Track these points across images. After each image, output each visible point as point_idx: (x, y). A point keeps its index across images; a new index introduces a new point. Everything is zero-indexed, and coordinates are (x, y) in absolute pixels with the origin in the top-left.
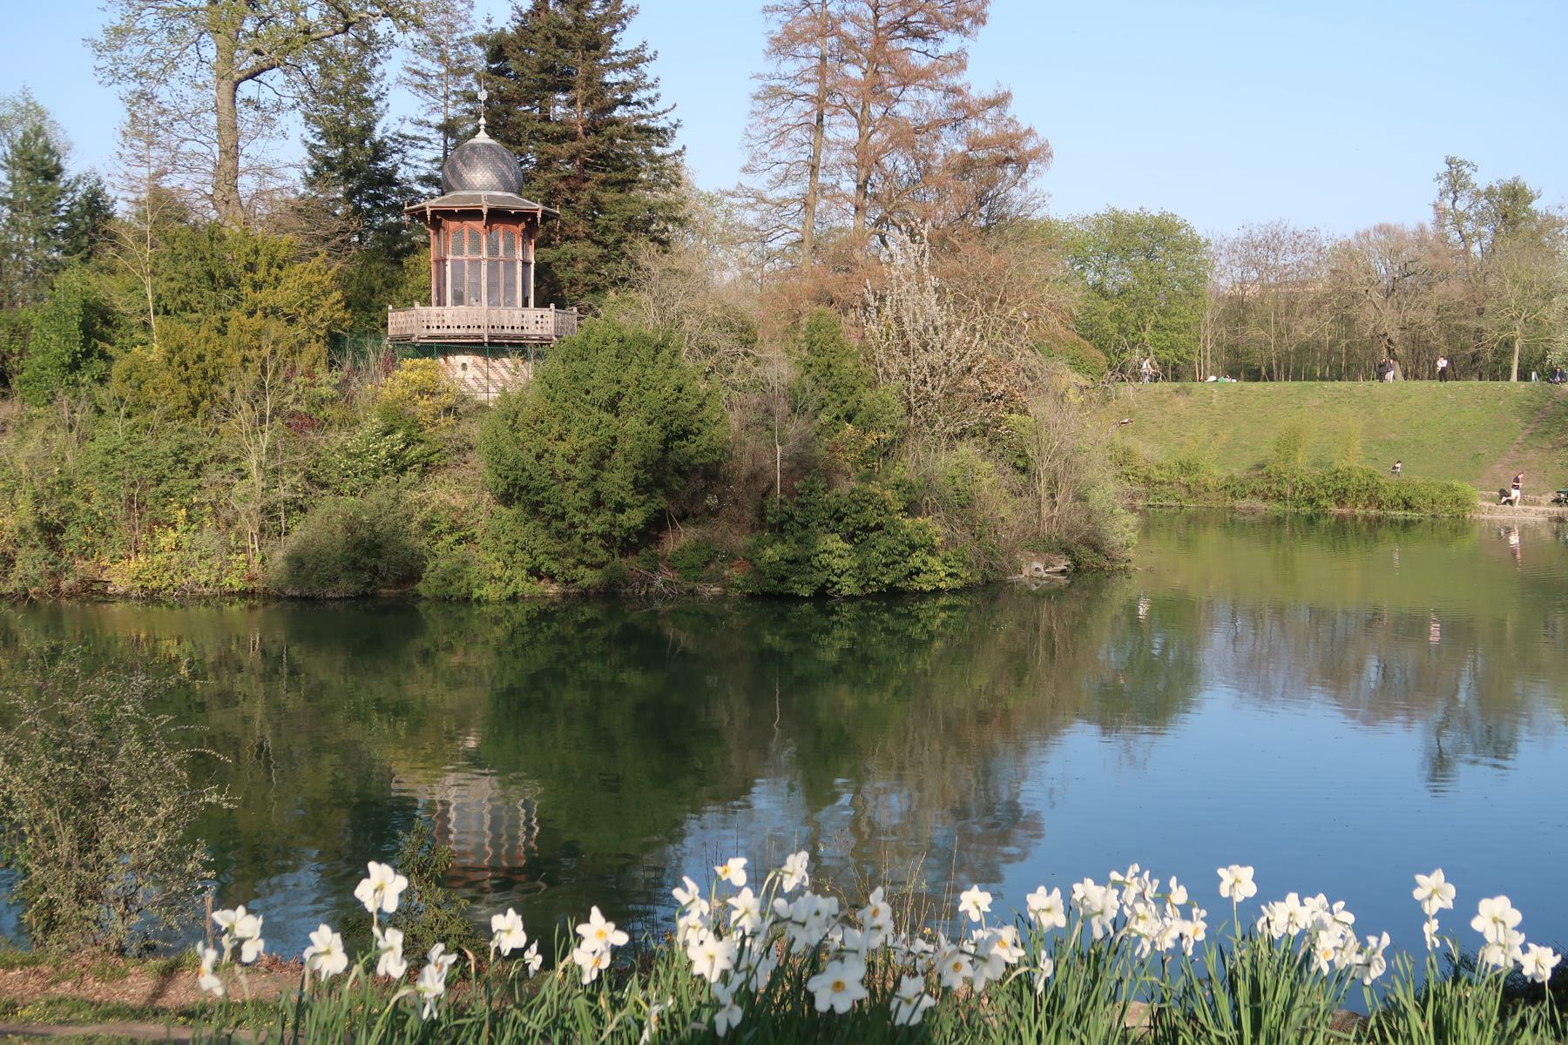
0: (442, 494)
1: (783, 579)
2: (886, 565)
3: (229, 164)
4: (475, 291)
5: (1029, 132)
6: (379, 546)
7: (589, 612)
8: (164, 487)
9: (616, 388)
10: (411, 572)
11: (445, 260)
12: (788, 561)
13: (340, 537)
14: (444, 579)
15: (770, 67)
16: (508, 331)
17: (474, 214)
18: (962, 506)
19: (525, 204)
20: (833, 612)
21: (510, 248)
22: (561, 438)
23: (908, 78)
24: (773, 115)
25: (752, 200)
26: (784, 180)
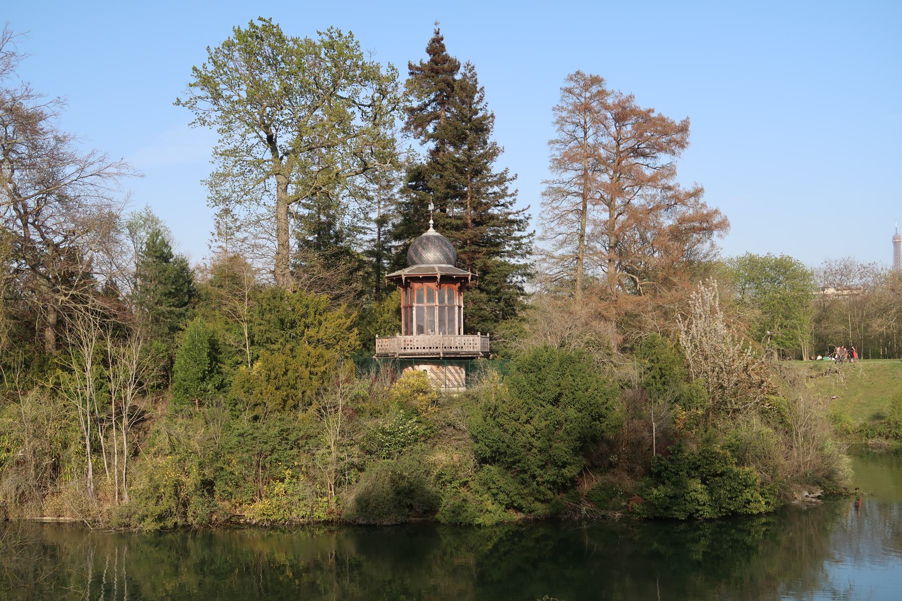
0: (442, 457)
1: (667, 509)
2: (730, 499)
3: (285, 252)
4: (432, 326)
5: (716, 212)
6: (412, 491)
7: (542, 531)
8: (275, 456)
9: (558, 390)
10: (431, 506)
11: (411, 307)
12: (670, 498)
13: (387, 486)
14: (453, 512)
15: (555, 176)
16: (453, 350)
17: (432, 279)
18: (763, 457)
19: (461, 272)
20: (698, 529)
21: (451, 298)
22: (527, 422)
23: (640, 181)
24: (555, 205)
25: (544, 257)
26: (562, 244)
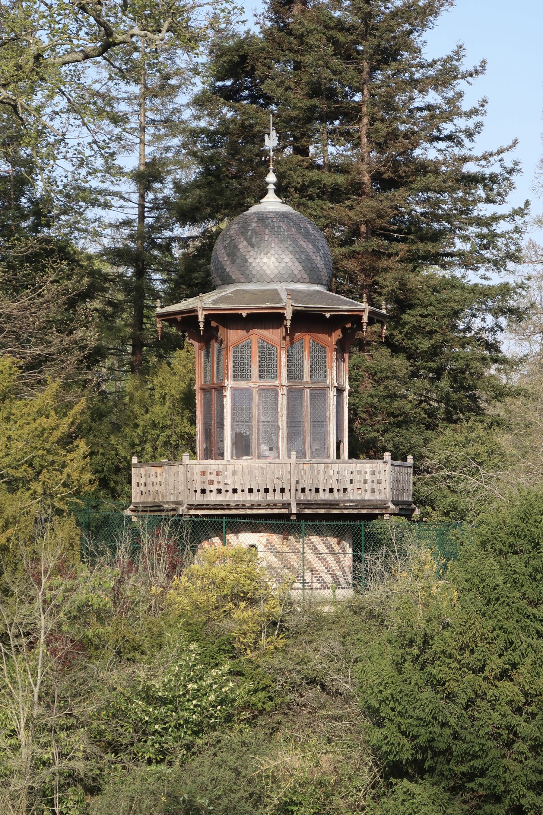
11: (220, 389)
16: (324, 496)
17: (272, 319)
19: (344, 304)
21: (318, 368)
22: (504, 675)
